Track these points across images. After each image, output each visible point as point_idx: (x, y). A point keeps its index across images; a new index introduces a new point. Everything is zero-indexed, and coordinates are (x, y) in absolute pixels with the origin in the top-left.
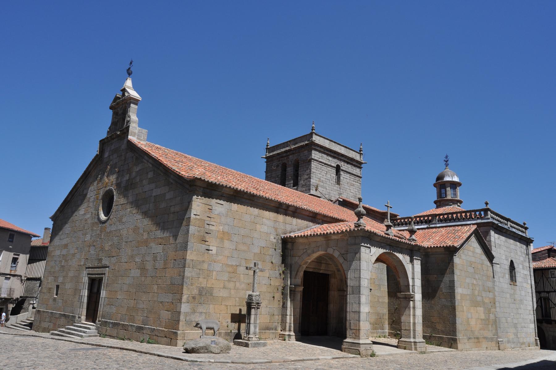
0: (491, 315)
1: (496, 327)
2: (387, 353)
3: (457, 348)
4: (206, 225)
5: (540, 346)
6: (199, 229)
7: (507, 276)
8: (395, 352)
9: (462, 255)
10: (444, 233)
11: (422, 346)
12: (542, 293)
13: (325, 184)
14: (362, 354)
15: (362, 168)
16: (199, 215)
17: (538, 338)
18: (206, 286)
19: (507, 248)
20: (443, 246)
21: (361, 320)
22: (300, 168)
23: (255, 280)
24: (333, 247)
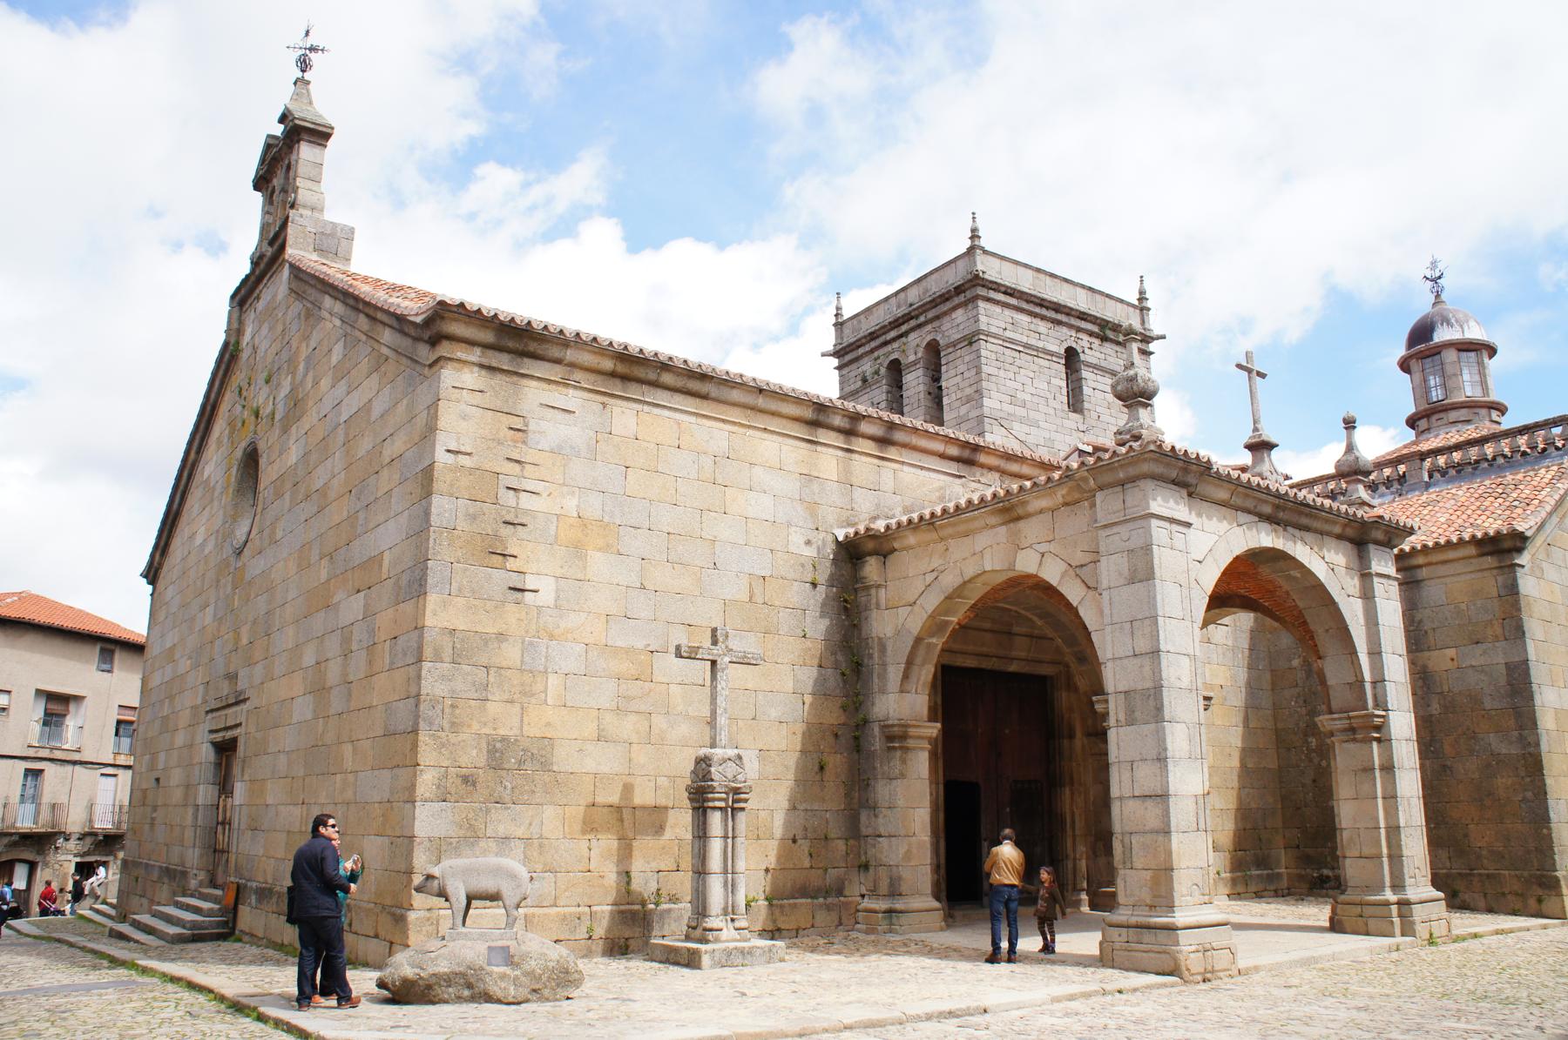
2: (1295, 956)
4: (502, 491)
6: (473, 508)
8: (1328, 951)
9: (1544, 565)
10: (1463, 499)
11: (1434, 917)
13: (1032, 413)
14: (1188, 970)
15: (1151, 353)
16: (469, 454)
18: (518, 732)
20: (1474, 537)
21: (1172, 829)
22: (944, 369)
23: (720, 700)
24: (1036, 547)
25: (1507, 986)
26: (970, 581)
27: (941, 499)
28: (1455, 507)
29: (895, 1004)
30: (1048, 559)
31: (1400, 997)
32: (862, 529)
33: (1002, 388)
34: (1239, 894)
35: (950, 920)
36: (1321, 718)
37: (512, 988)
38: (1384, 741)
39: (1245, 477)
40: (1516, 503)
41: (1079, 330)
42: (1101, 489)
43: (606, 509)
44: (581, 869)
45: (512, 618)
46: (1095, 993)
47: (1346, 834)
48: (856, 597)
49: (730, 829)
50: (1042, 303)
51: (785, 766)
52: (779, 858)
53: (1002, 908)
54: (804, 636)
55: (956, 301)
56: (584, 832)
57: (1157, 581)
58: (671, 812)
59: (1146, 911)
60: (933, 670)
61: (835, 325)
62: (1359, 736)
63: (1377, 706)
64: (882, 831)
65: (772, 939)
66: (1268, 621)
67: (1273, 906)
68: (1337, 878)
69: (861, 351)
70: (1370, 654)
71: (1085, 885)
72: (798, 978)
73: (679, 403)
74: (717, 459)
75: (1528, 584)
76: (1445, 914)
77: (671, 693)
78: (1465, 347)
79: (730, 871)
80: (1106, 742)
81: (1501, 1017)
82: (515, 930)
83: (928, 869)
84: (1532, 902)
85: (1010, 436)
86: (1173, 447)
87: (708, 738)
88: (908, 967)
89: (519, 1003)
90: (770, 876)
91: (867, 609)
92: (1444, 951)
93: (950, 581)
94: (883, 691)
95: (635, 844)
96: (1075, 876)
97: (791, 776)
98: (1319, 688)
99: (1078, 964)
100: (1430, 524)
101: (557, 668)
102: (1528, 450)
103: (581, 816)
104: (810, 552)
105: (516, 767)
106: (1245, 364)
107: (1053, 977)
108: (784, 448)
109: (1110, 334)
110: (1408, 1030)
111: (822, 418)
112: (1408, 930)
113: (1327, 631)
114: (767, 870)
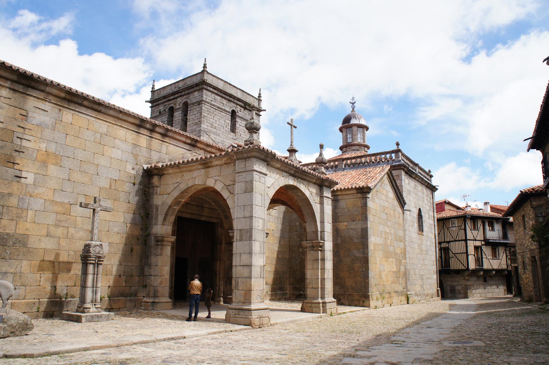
0: (401, 266)
1: (406, 278)
2: (289, 320)
3: (369, 306)
5: (440, 296)
7: (416, 225)
8: (299, 318)
9: (375, 198)
10: (354, 175)
11: (333, 307)
12: (443, 243)
13: (218, 131)
14: (254, 324)
15: (261, 115)
17: (439, 289)
18: (14, 232)
19: (416, 194)
20: (356, 187)
22: (189, 112)
23: (95, 223)
25: (351, 328)
26: (191, 187)
27: (183, 158)
28: (351, 177)
29: (152, 335)
30: (218, 182)
31: (320, 332)
32: (153, 165)
33: (208, 121)
34: (273, 299)
35: (175, 306)
36: (304, 242)
37: (2, 332)
38: (323, 251)
39: (286, 160)
40: (369, 178)
41: (237, 104)
42: (238, 159)
43: (57, 149)
44: (36, 285)
45: (15, 187)
46: (223, 332)
47: (308, 281)
48: (149, 189)
49: (96, 271)
50: (226, 93)
51: (119, 249)
52: (114, 282)
53: (194, 303)
54: (129, 203)
55: (196, 89)
56: (38, 271)
57: (254, 193)
58: (74, 264)
59: (242, 304)
60: (174, 218)
61: (151, 91)
62: (315, 249)
63: (321, 239)
64: (152, 274)
65: (109, 312)
66: (290, 209)
67: (284, 303)
68: (305, 295)
69: (160, 102)
70: (321, 222)
71: (222, 295)
72: (118, 326)
73: (89, 113)
74: (102, 135)
75: (370, 204)
76: (336, 306)
77: (77, 220)
78: (360, 126)
79: (95, 287)
80: (232, 246)
81: (348, 337)
82: (6, 309)
83: (168, 288)
84: (361, 302)
85: (209, 138)
86: (263, 148)
87: (90, 237)
88: (158, 322)
89: (5, 338)
90: (110, 289)
91: (153, 194)
92: (335, 318)
93: (183, 187)
94: (156, 224)
95: (59, 276)
96: (219, 292)
97: (120, 253)
98: (304, 232)
99: (218, 322)
100: (343, 182)
101: (32, 208)
102: (374, 161)
103: (38, 264)
104: (134, 172)
105: (12, 245)
106: (290, 123)
107: (209, 326)
108: (128, 134)
109: (247, 107)
110: (321, 343)
111: (142, 124)
112: (325, 311)
113: (308, 214)
114: (109, 287)
